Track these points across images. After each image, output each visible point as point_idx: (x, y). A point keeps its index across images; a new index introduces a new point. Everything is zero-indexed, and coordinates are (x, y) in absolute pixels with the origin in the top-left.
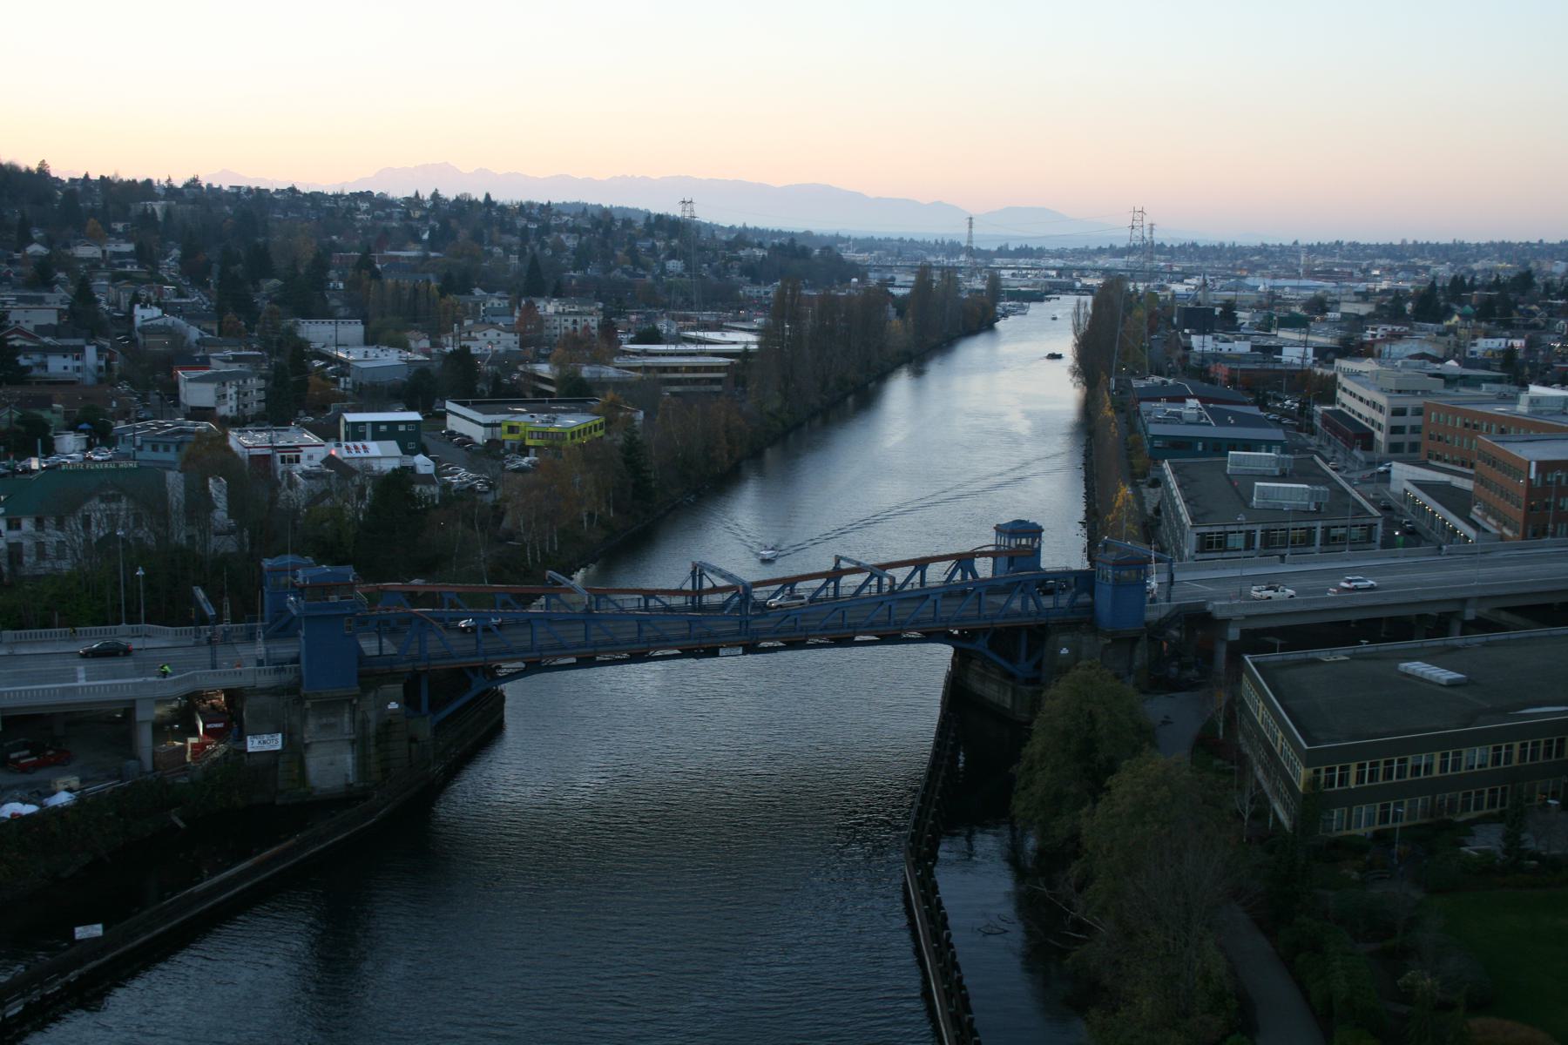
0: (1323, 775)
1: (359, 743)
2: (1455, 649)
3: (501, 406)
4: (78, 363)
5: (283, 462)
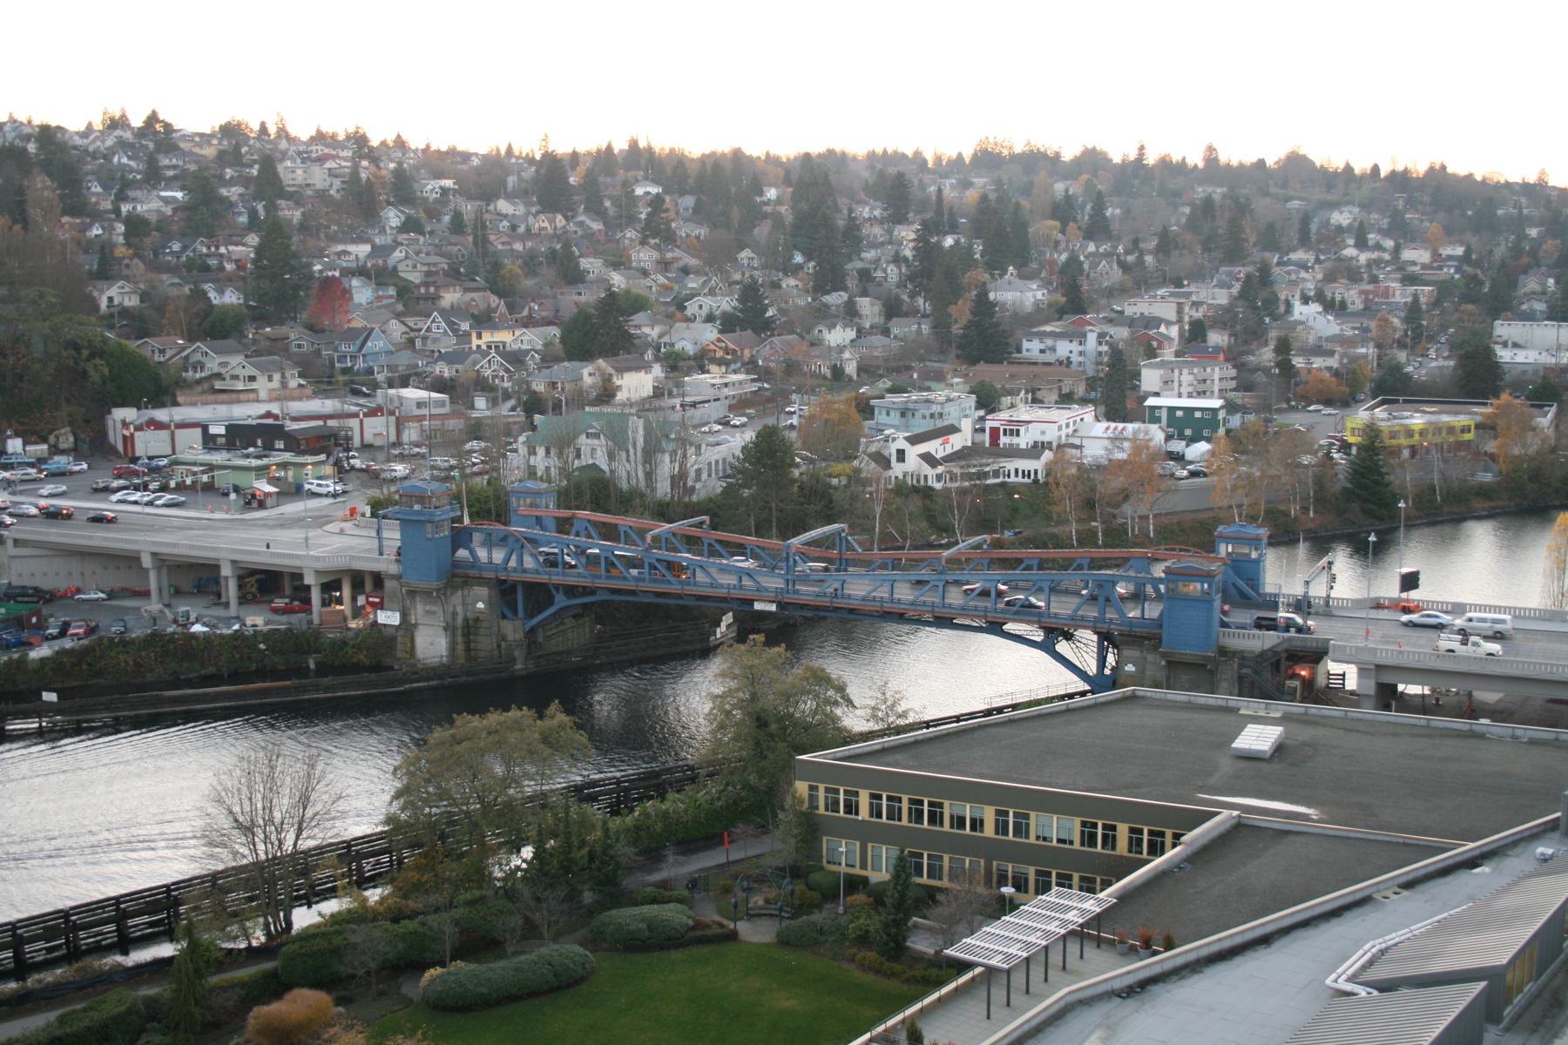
0: (821, 794)
1: (449, 628)
2: (1481, 736)
3: (1416, 405)
4: (1080, 348)
5: (1005, 434)
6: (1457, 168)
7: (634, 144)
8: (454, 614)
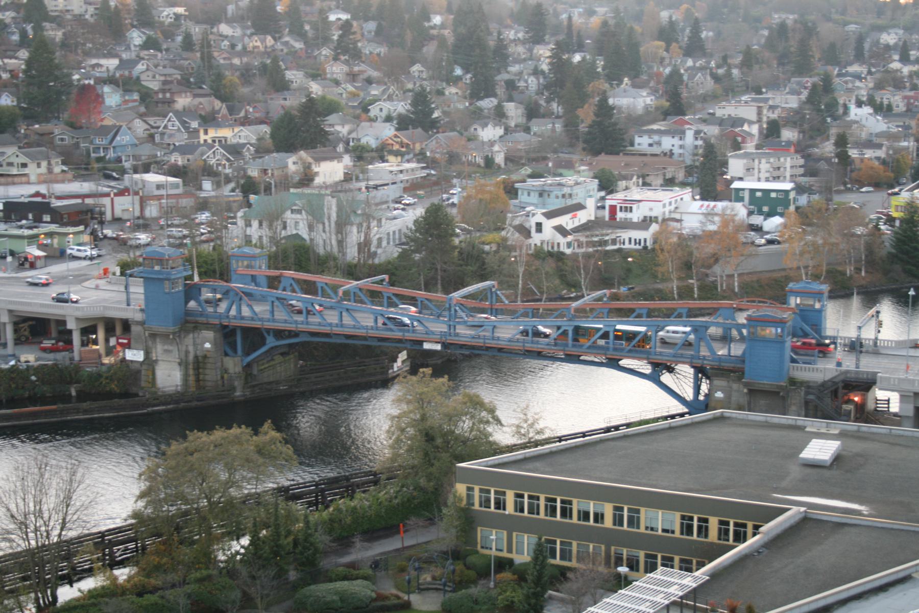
1: (183, 364)
7: (539, 6)
8: (187, 352)
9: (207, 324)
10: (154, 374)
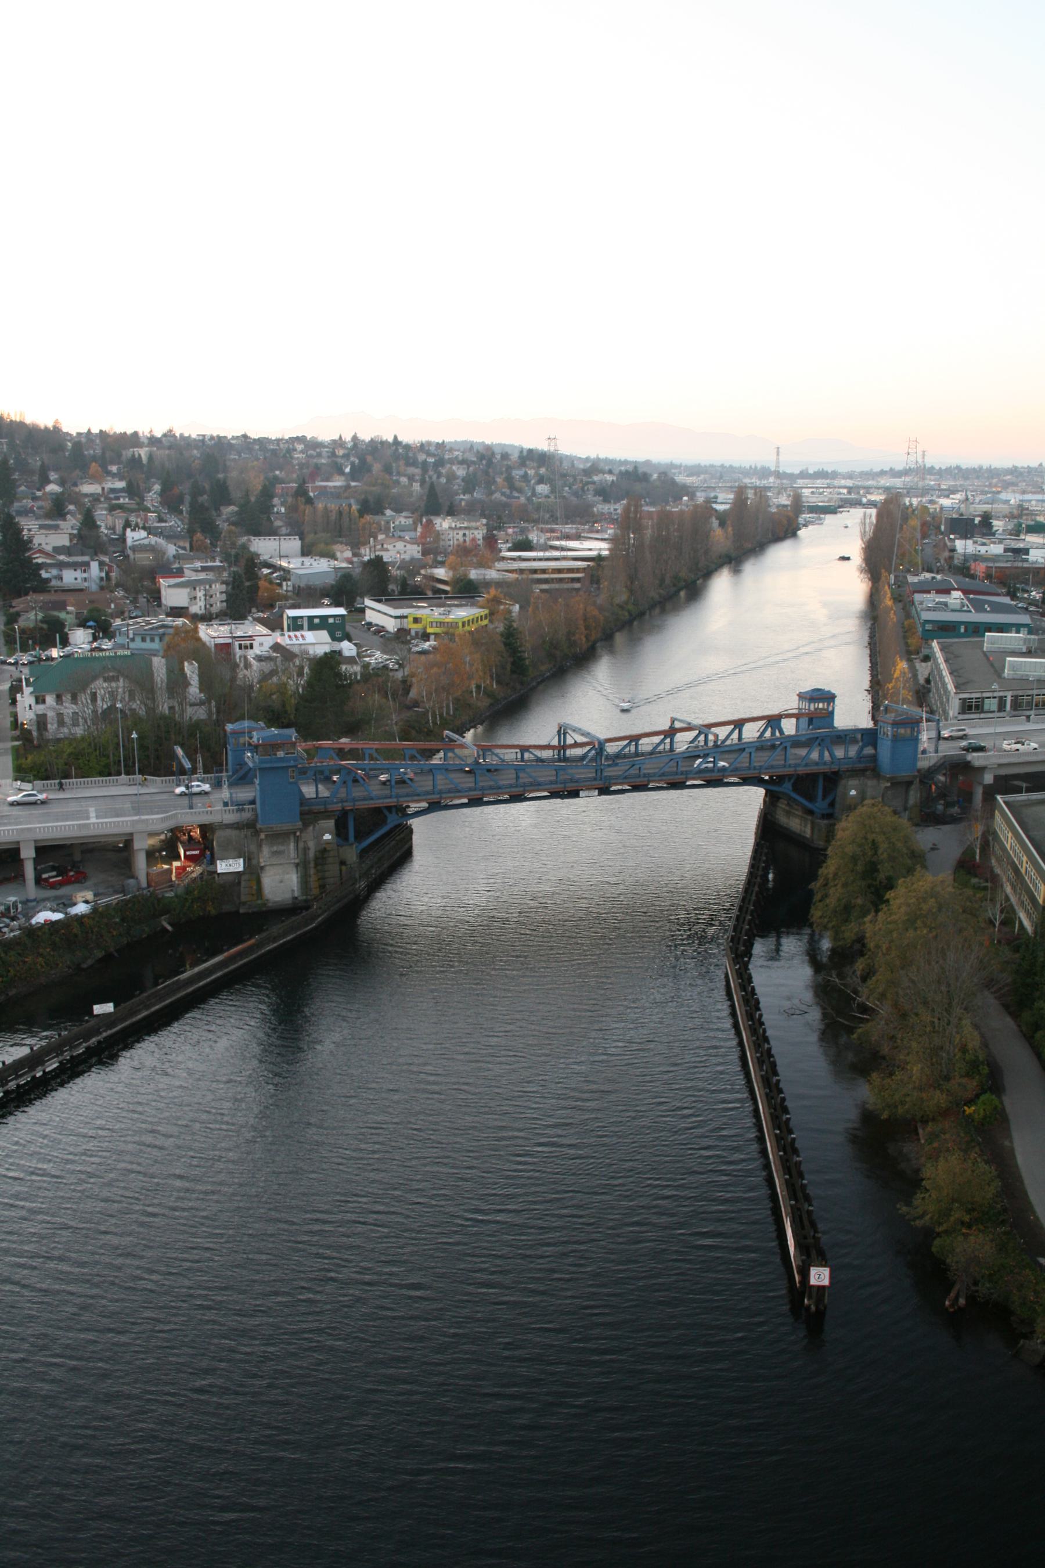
1: (302, 866)
6: (458, 440)
7: (101, 431)
8: (306, 849)
9: (326, 812)
10: (259, 882)
